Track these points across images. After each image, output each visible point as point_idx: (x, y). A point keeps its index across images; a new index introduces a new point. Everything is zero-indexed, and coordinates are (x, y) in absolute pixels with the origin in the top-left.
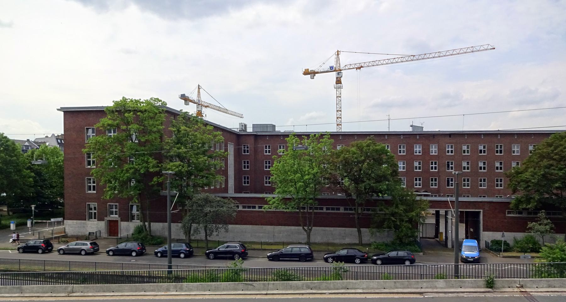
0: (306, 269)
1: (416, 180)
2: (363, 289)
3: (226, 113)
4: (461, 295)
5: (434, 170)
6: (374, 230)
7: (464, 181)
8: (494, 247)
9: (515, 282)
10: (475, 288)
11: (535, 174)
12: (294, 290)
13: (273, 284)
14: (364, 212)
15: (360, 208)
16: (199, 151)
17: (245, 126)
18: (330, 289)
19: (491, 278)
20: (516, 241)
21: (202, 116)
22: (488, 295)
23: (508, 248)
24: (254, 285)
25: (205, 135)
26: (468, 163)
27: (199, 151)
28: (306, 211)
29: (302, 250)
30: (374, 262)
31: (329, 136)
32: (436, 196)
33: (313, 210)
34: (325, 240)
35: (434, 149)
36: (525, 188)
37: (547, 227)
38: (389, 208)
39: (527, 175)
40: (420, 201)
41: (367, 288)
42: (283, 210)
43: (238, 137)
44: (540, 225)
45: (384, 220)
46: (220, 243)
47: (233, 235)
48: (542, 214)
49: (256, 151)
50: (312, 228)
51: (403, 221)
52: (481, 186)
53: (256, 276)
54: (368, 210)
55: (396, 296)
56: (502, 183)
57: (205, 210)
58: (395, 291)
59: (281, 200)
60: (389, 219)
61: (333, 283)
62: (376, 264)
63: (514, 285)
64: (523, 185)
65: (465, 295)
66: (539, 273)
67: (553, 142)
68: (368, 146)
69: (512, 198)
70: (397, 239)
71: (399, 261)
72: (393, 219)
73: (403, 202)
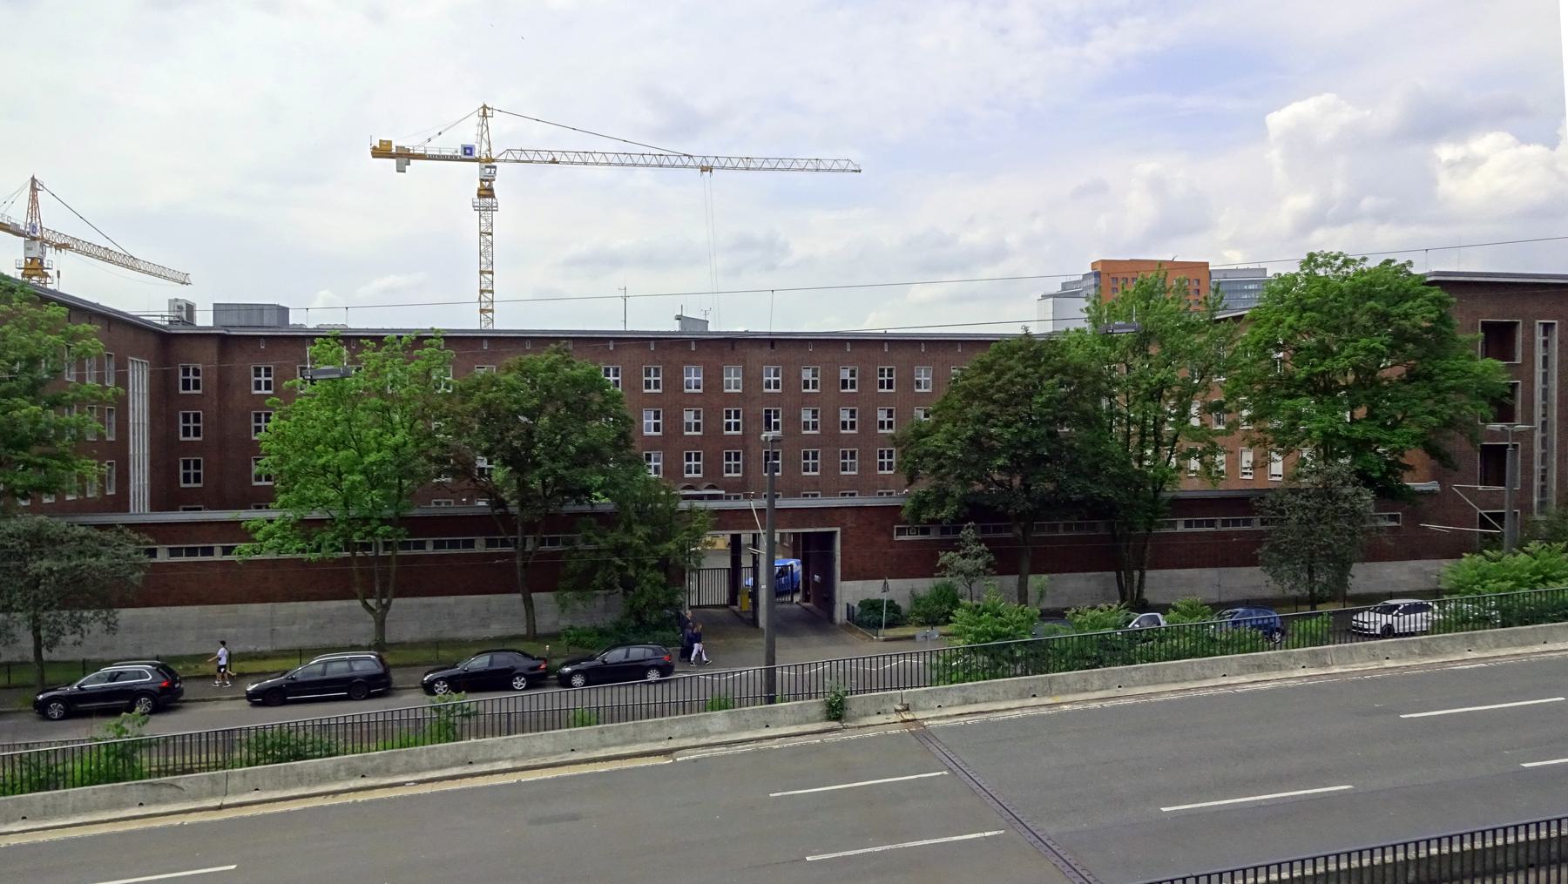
0: (357, 720)
1: (689, 459)
2: (513, 759)
3: (133, 268)
4: (766, 744)
5: (732, 432)
6: (568, 595)
7: (882, 457)
8: (866, 618)
9: (892, 699)
10: (801, 723)
11: (955, 436)
12: (310, 784)
13: (244, 774)
14: (541, 548)
15: (530, 538)
16: (14, 384)
17: (190, 309)
18: (418, 771)
19: (837, 695)
20: (916, 600)
21: (47, 275)
22: (830, 737)
23: (896, 617)
24: (181, 784)
25: (38, 334)
26: (814, 412)
27: (14, 384)
28: (371, 554)
29: (357, 667)
30: (565, 681)
31: (442, 342)
32: (737, 498)
33: (394, 550)
34: (429, 633)
35: (733, 379)
36: (934, 471)
37: (980, 561)
38: (608, 533)
39: (937, 441)
40: (690, 511)
41: (526, 755)
42: (299, 555)
43: (166, 344)
44: (964, 556)
45: (594, 567)
46: (86, 667)
47: (129, 645)
48: (968, 532)
49: (223, 385)
50: (389, 602)
51: (644, 566)
52: (844, 469)
53: (196, 757)
54: (553, 542)
55: (602, 768)
56: (893, 460)
57: (31, 566)
58: (602, 753)
59: (294, 526)
60: (609, 563)
61: (428, 751)
62: (571, 686)
63: (890, 707)
64: (931, 463)
65: (775, 745)
66: (946, 673)
67: (993, 362)
68: (552, 368)
69: (900, 497)
70: (628, 616)
71: (631, 672)
72: (618, 561)
73: (644, 516)
